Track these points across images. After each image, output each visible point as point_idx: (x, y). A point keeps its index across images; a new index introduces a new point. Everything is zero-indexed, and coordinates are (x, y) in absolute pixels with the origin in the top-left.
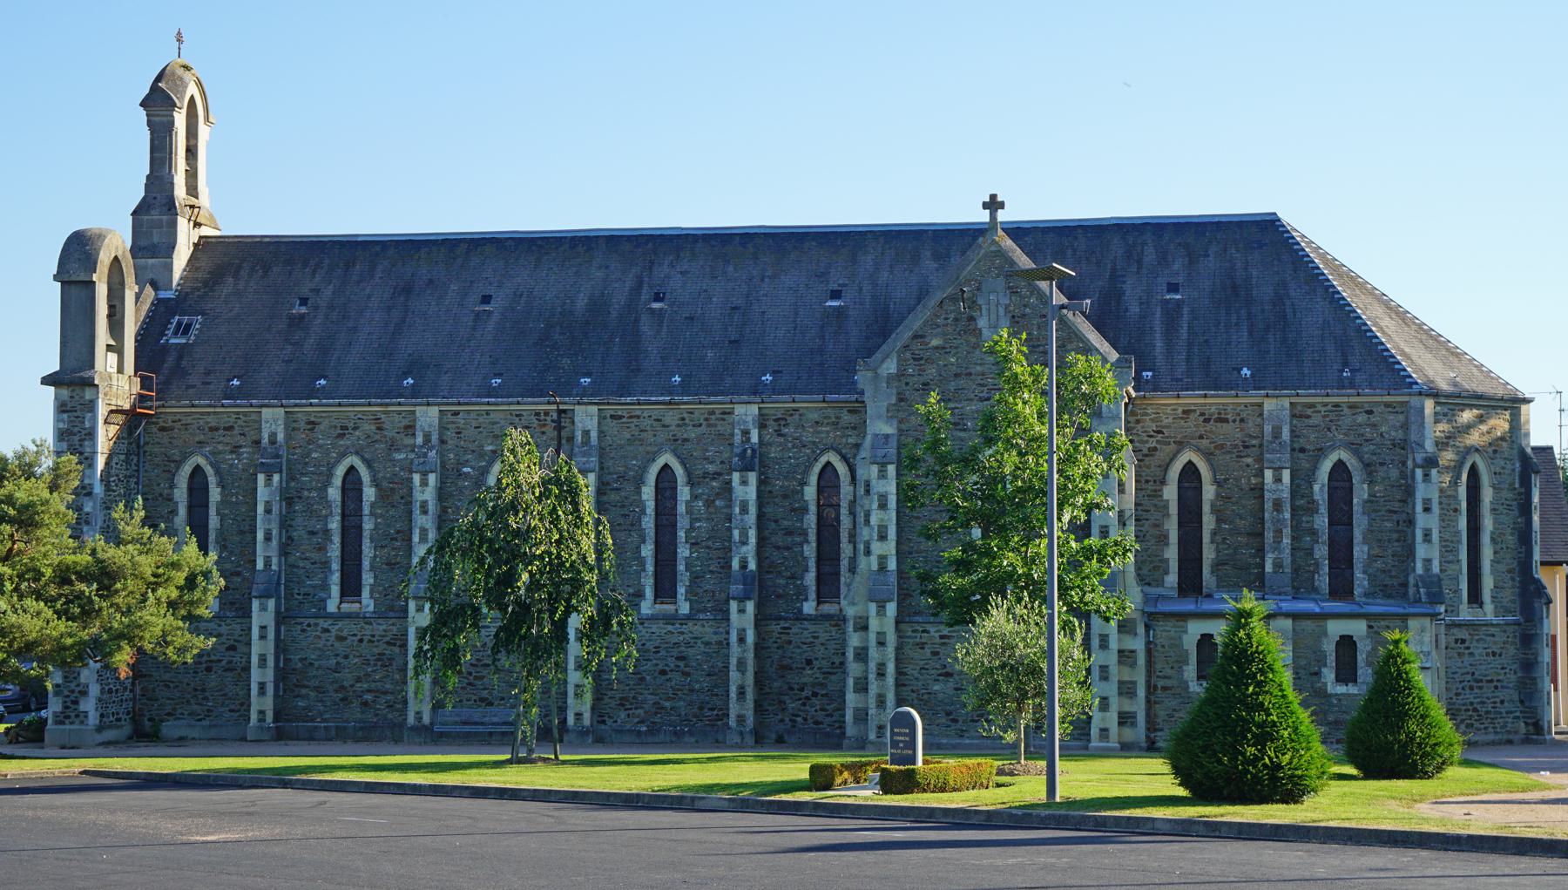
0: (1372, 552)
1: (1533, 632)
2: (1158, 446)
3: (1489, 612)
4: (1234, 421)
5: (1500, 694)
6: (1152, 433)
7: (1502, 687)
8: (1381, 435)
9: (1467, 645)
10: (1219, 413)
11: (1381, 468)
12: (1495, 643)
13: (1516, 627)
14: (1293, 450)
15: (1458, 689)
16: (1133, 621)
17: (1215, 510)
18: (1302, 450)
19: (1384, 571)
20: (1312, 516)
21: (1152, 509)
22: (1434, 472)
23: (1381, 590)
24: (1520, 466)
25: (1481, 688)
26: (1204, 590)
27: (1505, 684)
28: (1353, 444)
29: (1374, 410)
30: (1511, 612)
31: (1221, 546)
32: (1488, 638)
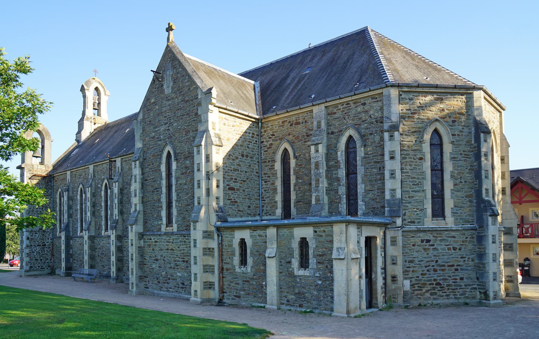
0: (367, 188)
1: (483, 234)
2: (273, 143)
3: (450, 221)
4: (302, 123)
5: (460, 274)
6: (271, 136)
7: (461, 269)
8: (370, 116)
9: (431, 243)
10: (296, 120)
11: (370, 137)
12: (456, 242)
13: (474, 231)
14: (328, 133)
15: (423, 271)
16: (212, 232)
17: (296, 173)
18: (333, 133)
19: (373, 199)
20: (337, 170)
21: (271, 175)
22: (396, 134)
23: (377, 211)
24: (475, 129)
25: (443, 270)
26: (292, 216)
27: (464, 267)
28: (356, 125)
29: (366, 102)
30: (469, 222)
31: (298, 192)
32: (450, 239)
